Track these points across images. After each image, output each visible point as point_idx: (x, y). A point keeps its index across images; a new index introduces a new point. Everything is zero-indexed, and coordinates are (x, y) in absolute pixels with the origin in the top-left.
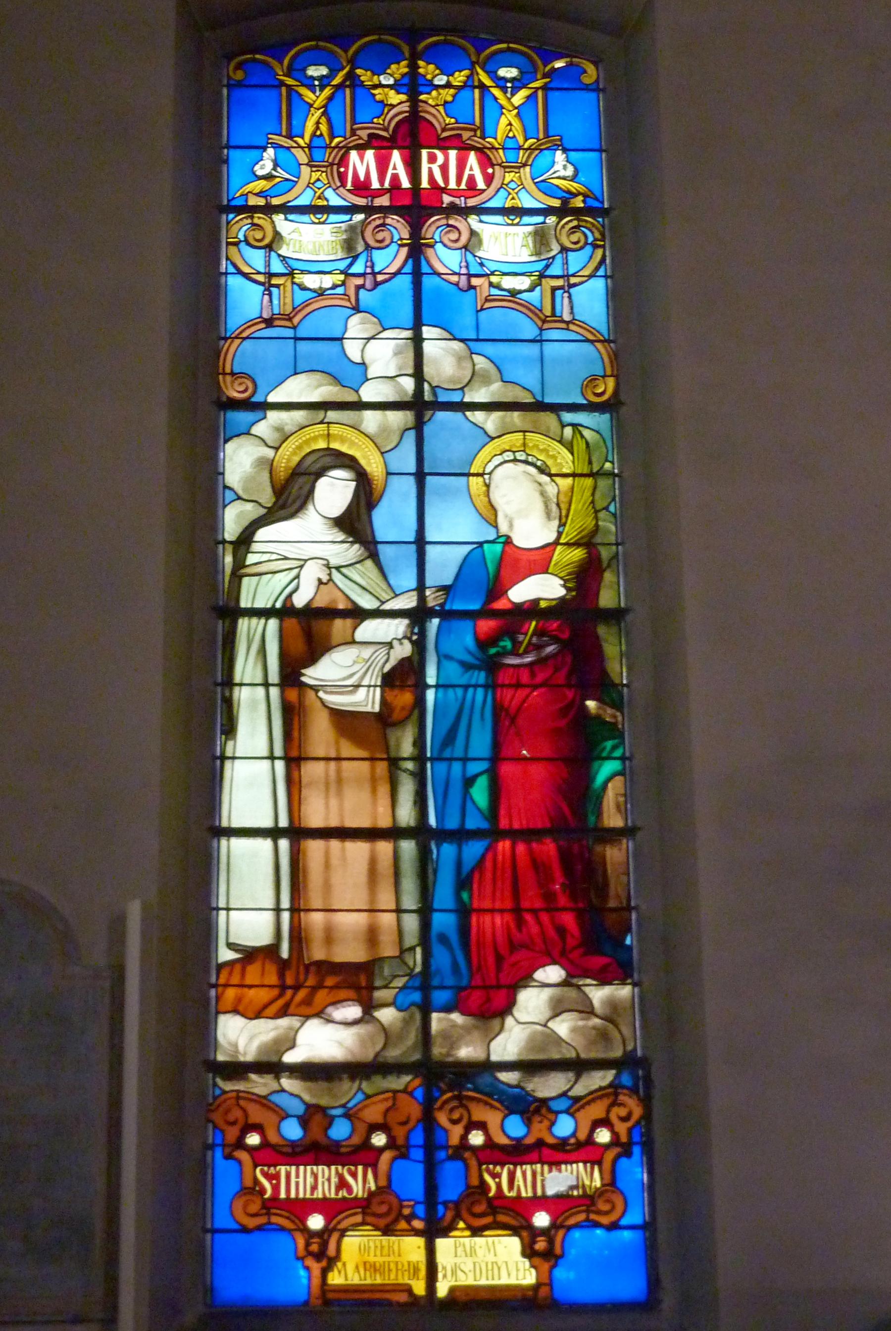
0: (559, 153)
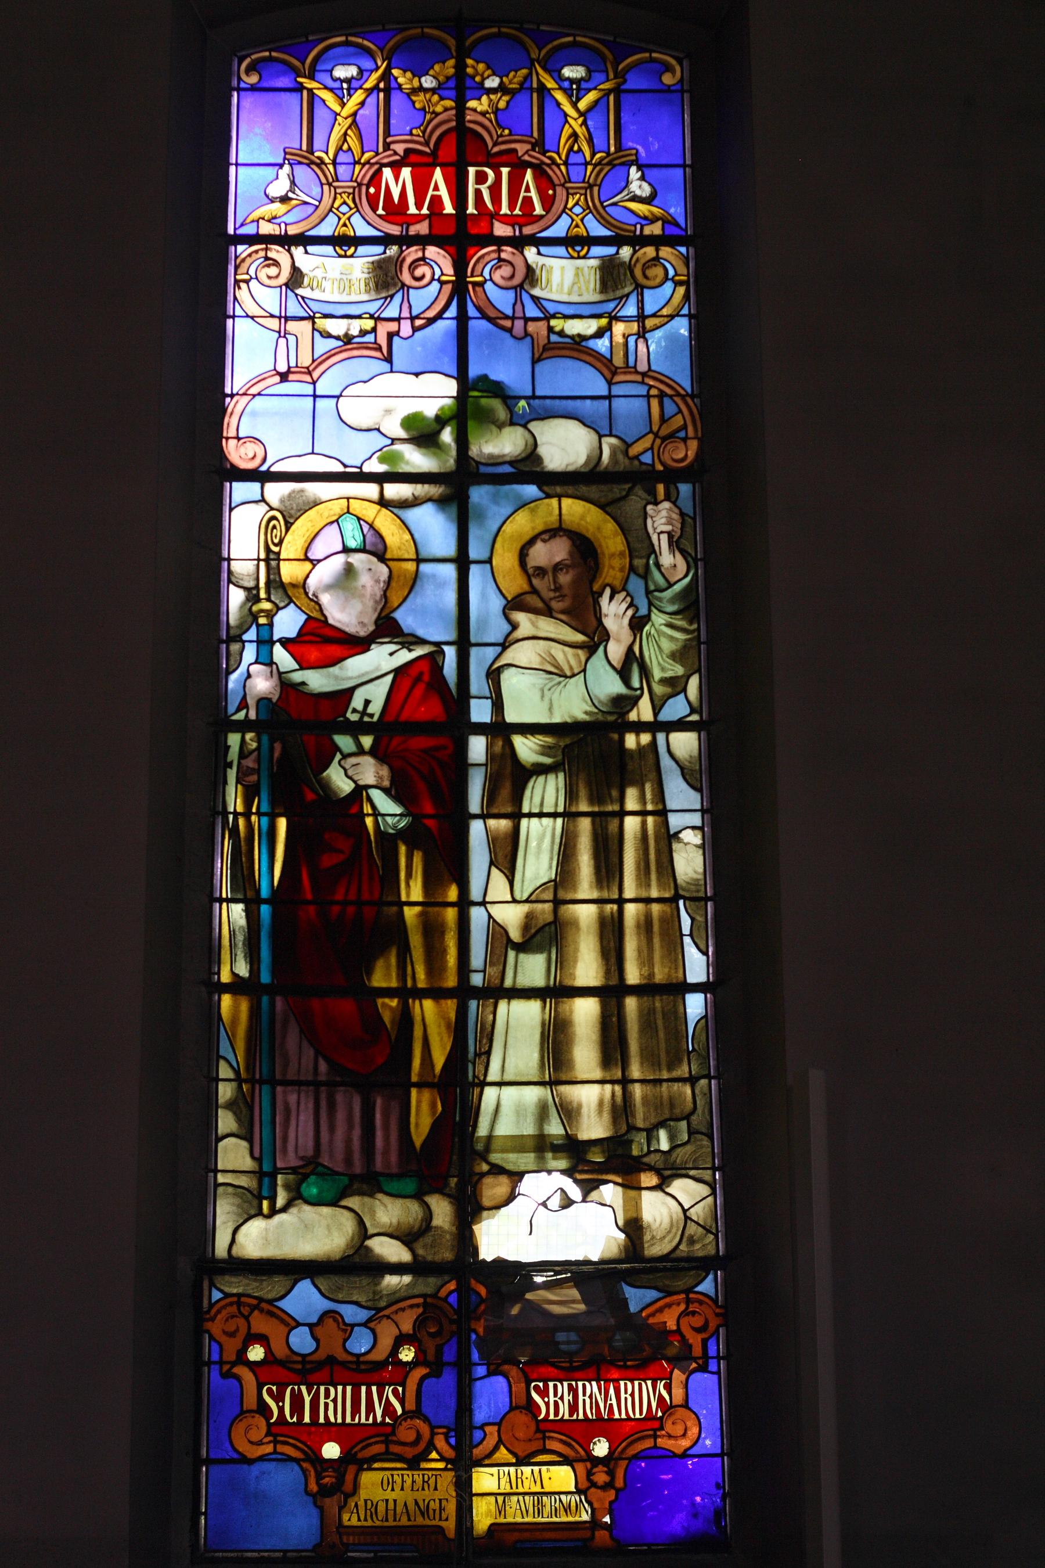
0: (633, 169)
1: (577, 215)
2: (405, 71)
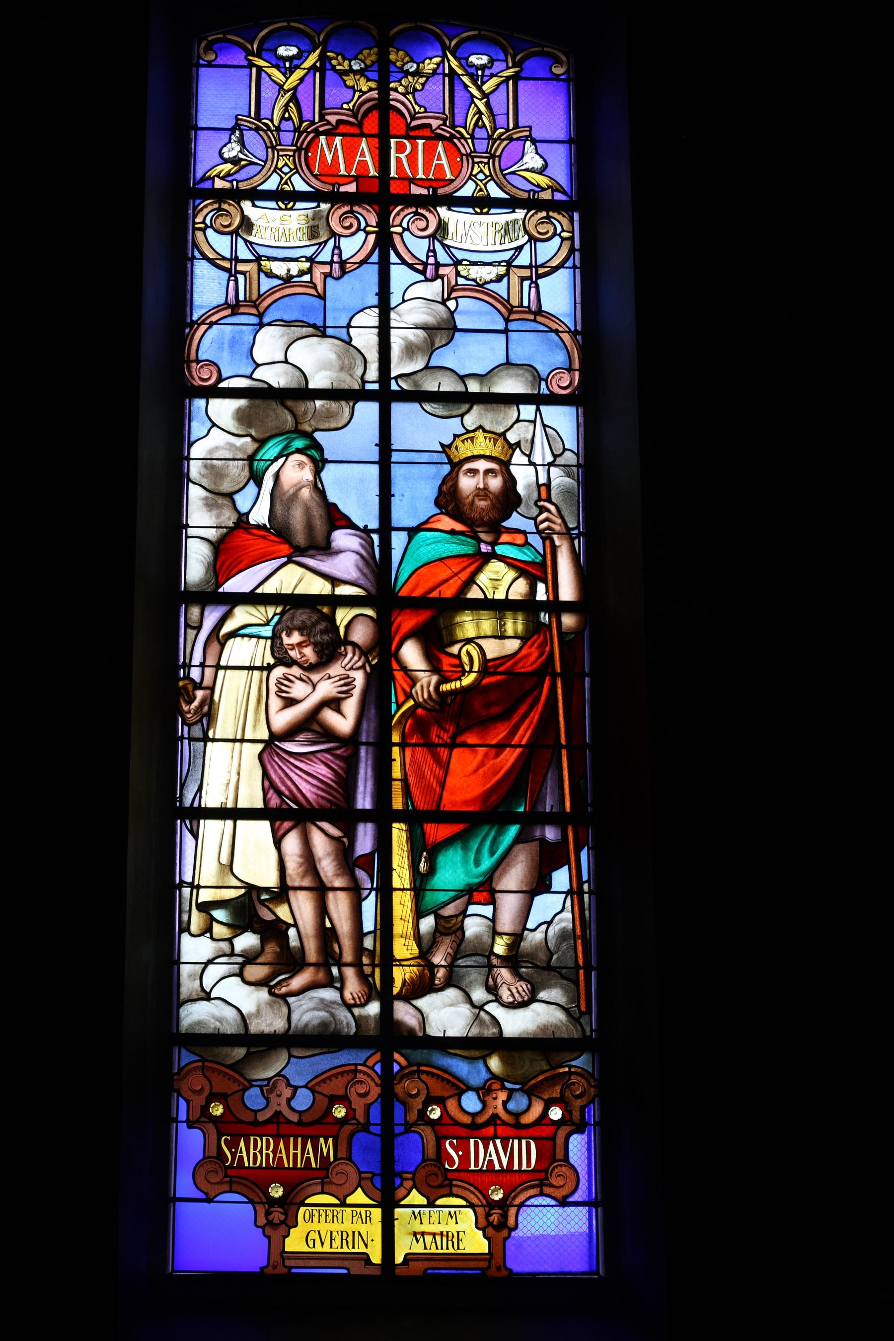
0: (528, 143)
1: (481, 181)
2: (338, 55)
